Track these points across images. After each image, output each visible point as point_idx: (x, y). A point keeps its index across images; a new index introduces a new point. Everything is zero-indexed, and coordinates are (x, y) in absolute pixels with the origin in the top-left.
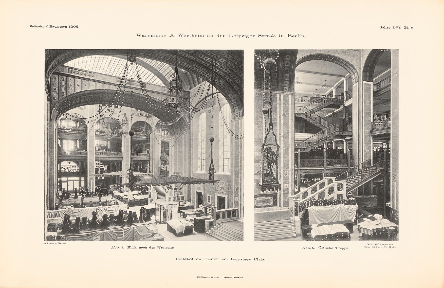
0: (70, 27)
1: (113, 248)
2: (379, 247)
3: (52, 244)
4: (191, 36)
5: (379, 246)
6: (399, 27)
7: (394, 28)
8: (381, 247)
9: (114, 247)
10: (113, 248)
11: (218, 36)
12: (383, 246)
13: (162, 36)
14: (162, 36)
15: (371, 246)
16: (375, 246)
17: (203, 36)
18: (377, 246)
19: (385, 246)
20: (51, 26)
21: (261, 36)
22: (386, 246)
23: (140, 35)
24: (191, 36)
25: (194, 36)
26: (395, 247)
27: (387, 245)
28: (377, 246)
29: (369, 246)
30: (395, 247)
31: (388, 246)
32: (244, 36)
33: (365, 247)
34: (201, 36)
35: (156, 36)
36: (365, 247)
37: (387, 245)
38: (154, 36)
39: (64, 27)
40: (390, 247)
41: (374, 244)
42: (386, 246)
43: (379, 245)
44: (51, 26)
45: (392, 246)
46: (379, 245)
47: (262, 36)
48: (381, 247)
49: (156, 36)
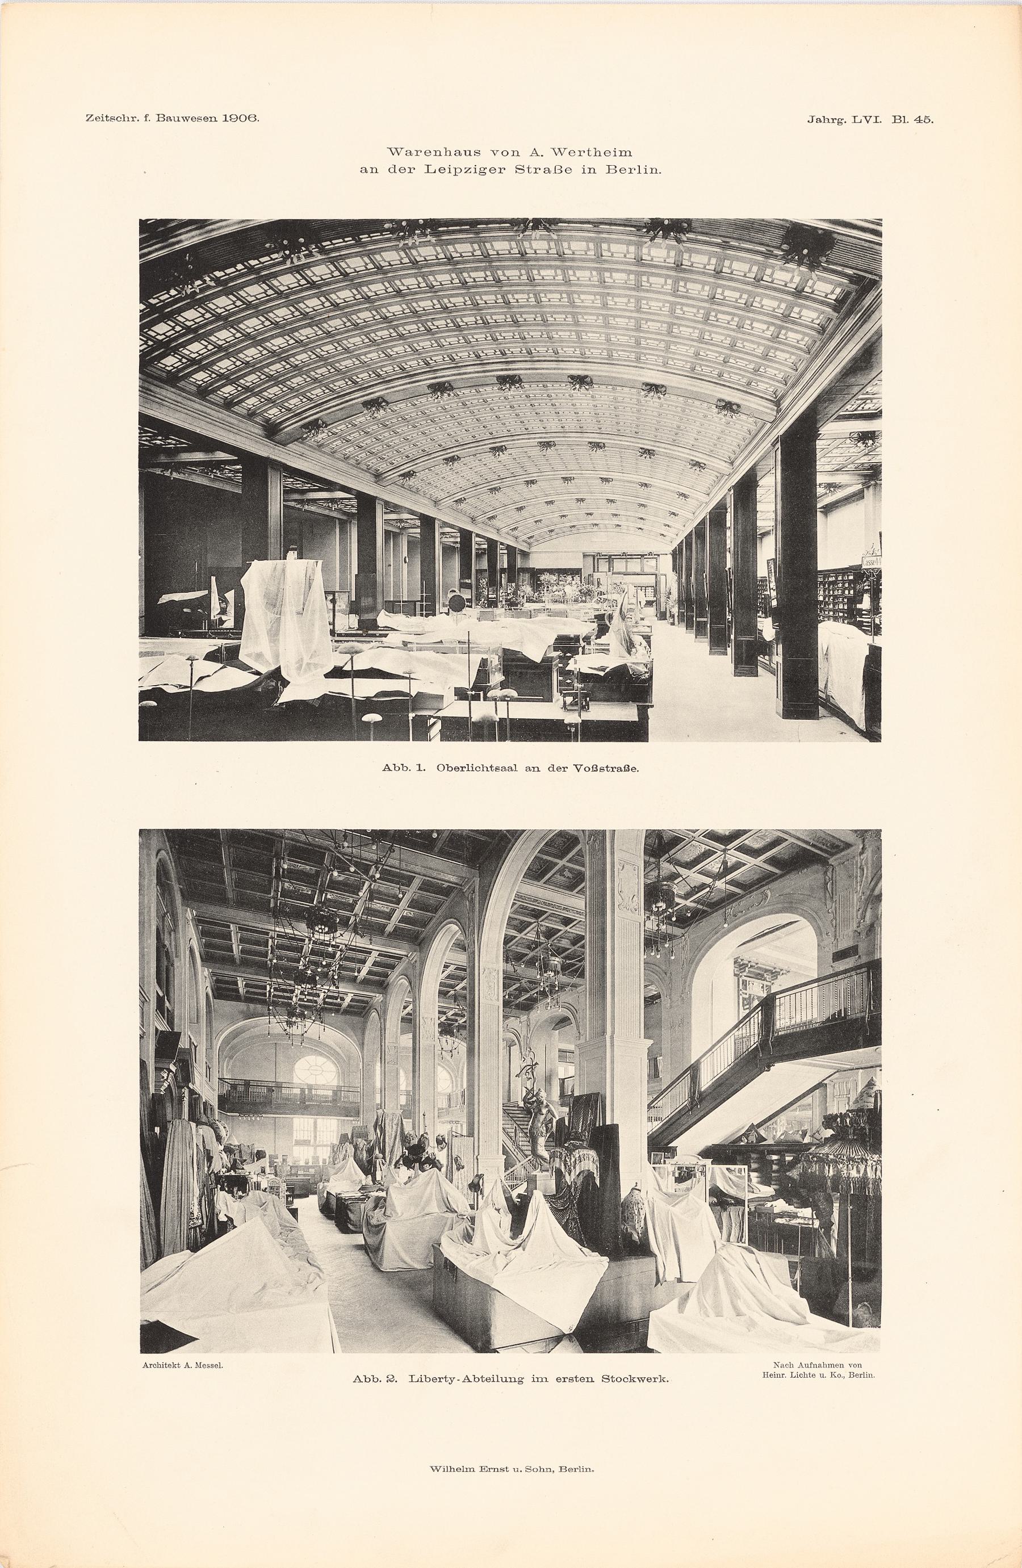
0: (228, 118)
1: (387, 768)
2: (814, 1375)
3: (174, 1366)
4: (592, 153)
5: (812, 1371)
6: (873, 119)
7: (858, 120)
8: (822, 1376)
9: (392, 767)
10: (387, 768)
11: (392, 170)
12: (827, 1371)
13: (468, 153)
14: (468, 153)
15: (787, 1371)
16: (801, 1371)
17: (628, 154)
18: (807, 1371)
19: (833, 1370)
20: (163, 118)
21: (522, 171)
22: (838, 1371)
23: (562, 150)
24: (592, 153)
25: (602, 154)
26: (870, 1376)
27: (842, 1366)
28: (807, 1371)
29: (779, 1371)
30: (870, 1376)
31: (845, 1372)
32: (473, 170)
33: (766, 1375)
34: (623, 154)
35: (448, 153)
36: (766, 1375)
37: (842, 1366)
38: (443, 153)
39: (206, 119)
40: (852, 1375)
41: (796, 1365)
42: (838, 1371)
43: (815, 1366)
44: (163, 118)
45: (858, 1371)
46: (815, 1366)
47: (526, 170)
48: (822, 1376)
49: (448, 153)
